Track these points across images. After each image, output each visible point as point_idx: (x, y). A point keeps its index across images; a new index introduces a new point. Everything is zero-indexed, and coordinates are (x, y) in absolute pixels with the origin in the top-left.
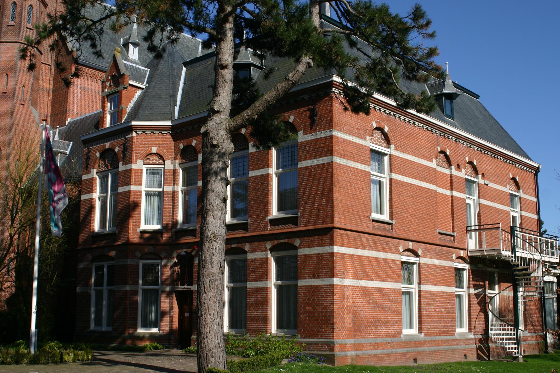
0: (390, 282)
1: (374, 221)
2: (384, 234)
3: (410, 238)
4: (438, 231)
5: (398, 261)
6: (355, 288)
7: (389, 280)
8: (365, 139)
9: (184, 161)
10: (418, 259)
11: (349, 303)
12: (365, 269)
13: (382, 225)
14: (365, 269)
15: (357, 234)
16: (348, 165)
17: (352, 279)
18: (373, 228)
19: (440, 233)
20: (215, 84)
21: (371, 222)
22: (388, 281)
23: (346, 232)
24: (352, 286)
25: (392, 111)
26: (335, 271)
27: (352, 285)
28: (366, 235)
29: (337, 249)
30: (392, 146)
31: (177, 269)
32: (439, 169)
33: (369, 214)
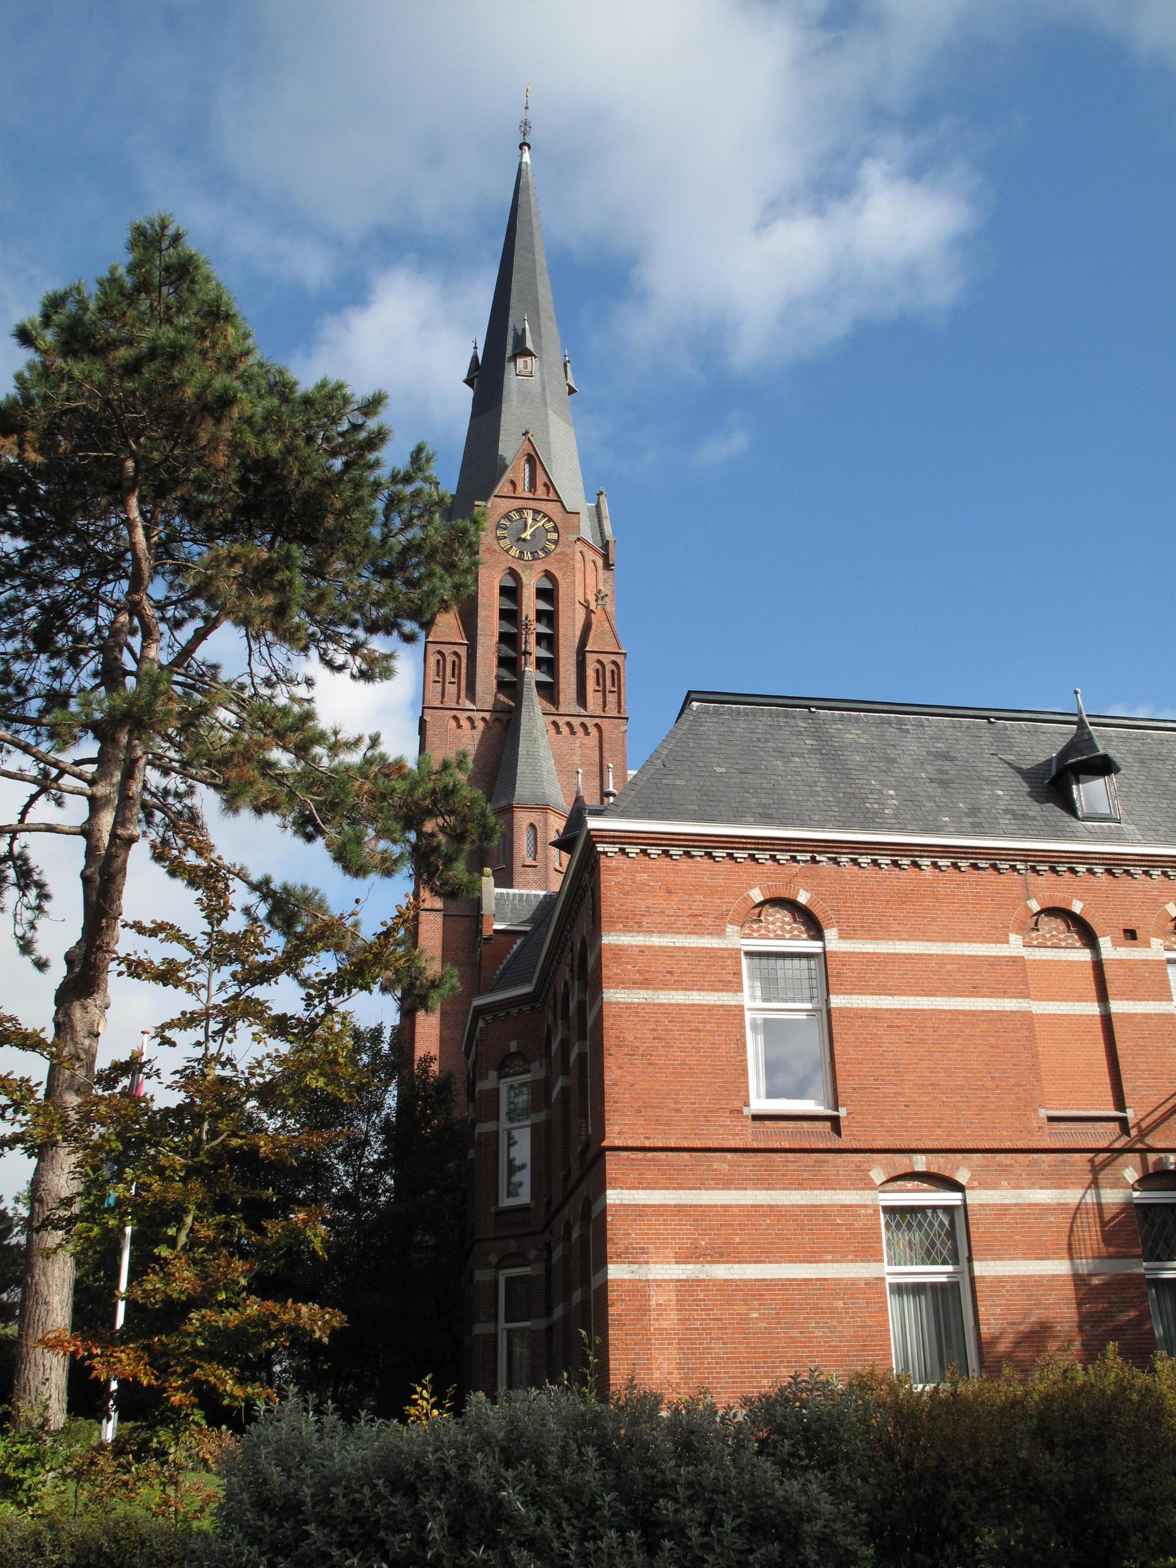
0: (832, 1261)
1: (756, 1118)
2: (778, 1148)
3: (914, 1145)
4: (1043, 1113)
5: (866, 1206)
6: (686, 1286)
7: (829, 1257)
8: (721, 933)
9: (203, 1024)
10: (959, 1195)
11: (670, 1321)
12: (713, 1236)
13: (805, 1124)
14: (713, 1236)
15: (695, 1156)
16: (657, 1001)
17: (677, 1263)
18: (755, 1136)
19: (1051, 1119)
20: (20, 1336)
21: (749, 1122)
22: (826, 1261)
23: (650, 1155)
24: (678, 1281)
25: (820, 853)
26: (611, 1249)
27: (675, 1277)
28: (729, 1155)
29: (1060, 1267)
30: (830, 934)
31: (100, 667)
32: (1027, 953)
33: (737, 1104)
